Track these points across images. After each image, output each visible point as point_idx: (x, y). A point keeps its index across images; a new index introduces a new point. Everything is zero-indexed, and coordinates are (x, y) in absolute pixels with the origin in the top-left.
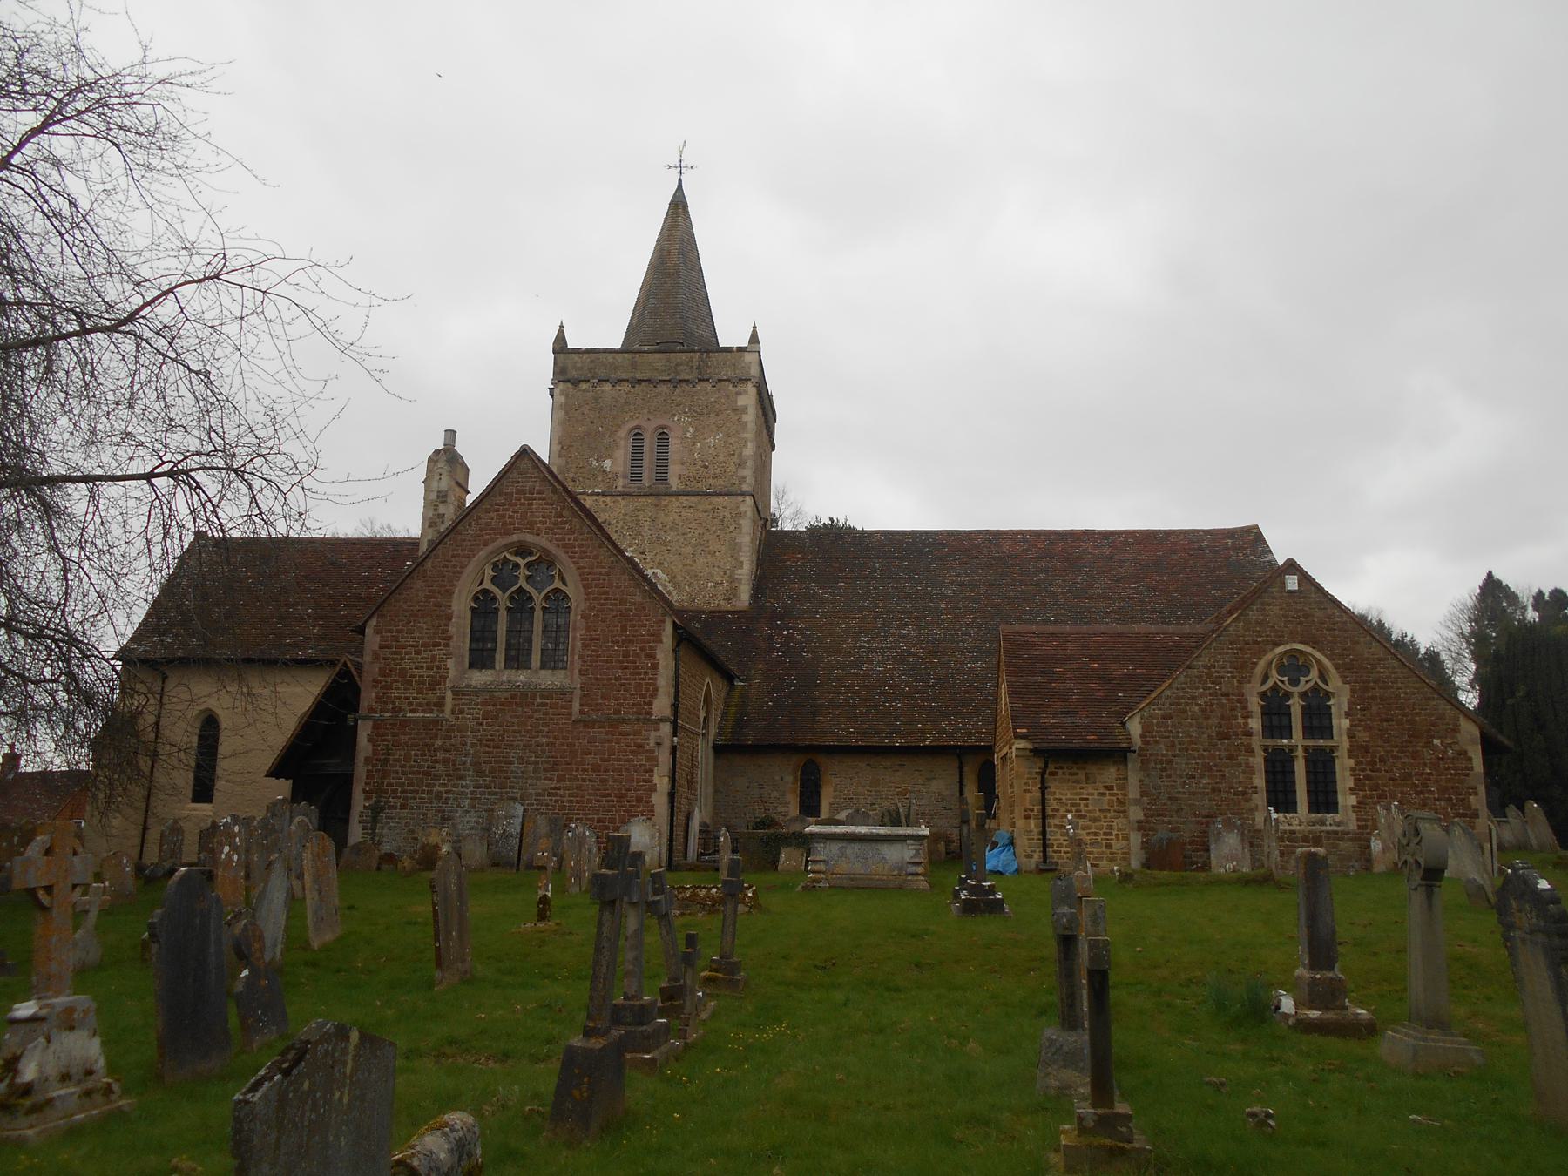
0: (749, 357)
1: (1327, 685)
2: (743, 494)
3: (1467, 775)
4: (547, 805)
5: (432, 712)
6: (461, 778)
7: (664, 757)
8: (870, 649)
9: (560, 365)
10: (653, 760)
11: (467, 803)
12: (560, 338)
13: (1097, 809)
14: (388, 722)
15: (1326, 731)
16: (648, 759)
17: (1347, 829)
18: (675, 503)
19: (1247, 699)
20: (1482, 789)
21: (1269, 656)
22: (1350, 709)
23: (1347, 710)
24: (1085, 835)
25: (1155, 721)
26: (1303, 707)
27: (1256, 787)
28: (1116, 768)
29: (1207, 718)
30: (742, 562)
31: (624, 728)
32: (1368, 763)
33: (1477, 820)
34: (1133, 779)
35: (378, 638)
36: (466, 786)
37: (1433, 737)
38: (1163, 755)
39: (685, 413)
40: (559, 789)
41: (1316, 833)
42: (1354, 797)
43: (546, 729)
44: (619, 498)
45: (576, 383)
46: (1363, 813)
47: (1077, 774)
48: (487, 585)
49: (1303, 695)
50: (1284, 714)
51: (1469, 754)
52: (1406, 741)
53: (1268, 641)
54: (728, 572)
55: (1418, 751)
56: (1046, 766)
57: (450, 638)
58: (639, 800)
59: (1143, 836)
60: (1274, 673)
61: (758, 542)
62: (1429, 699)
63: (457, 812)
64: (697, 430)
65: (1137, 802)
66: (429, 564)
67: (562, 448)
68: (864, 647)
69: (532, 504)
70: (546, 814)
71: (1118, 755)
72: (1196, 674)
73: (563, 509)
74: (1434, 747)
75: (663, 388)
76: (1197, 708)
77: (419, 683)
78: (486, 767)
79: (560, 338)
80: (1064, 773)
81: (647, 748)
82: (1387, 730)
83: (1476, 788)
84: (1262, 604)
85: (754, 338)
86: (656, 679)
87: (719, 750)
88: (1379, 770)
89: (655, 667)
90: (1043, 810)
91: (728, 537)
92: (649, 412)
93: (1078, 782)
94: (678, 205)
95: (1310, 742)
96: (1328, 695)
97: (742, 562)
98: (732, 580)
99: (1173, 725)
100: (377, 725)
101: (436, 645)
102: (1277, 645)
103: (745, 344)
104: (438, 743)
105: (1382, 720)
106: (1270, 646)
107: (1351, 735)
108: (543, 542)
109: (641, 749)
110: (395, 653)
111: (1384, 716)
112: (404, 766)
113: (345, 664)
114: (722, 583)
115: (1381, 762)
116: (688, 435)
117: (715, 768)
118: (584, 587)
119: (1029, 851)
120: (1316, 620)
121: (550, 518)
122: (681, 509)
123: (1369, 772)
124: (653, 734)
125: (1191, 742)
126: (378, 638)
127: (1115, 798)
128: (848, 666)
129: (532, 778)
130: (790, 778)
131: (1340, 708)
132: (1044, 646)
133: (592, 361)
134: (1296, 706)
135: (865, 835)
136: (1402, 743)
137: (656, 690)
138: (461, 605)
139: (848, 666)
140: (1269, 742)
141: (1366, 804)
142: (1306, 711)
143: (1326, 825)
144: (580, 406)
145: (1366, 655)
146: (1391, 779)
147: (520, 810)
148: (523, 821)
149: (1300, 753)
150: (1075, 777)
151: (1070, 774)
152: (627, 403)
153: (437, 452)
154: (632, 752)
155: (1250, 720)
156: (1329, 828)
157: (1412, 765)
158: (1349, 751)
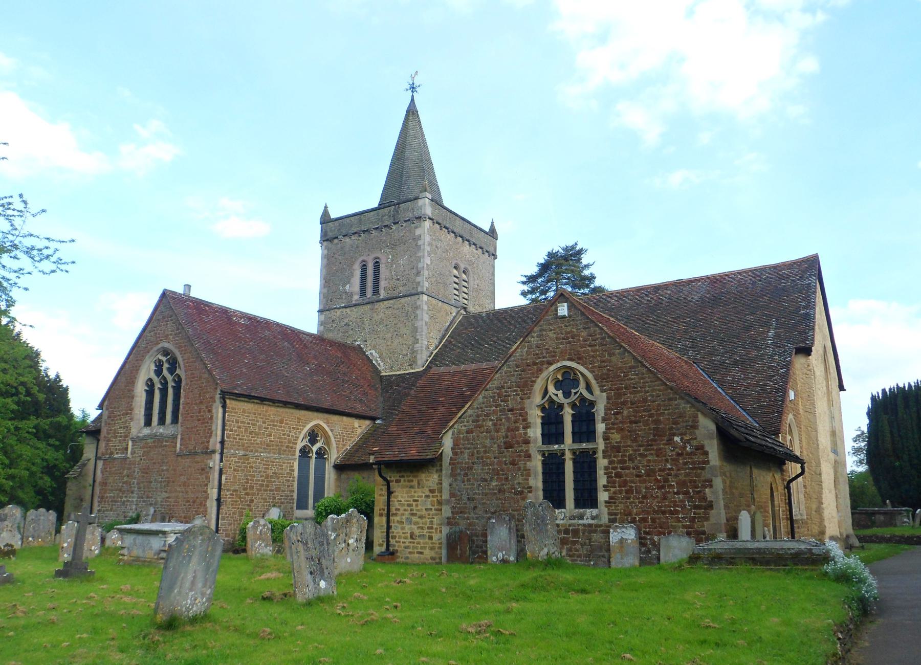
3: (703, 469)
6: (132, 492)
12: (326, 213)
13: (424, 508)
18: (382, 305)
19: (526, 413)
21: (544, 374)
22: (606, 414)
24: (416, 529)
25: (462, 436)
26: (573, 415)
27: (531, 487)
28: (438, 475)
29: (497, 431)
30: (418, 339)
32: (620, 462)
33: (712, 511)
37: (674, 435)
38: (466, 463)
41: (574, 526)
44: (353, 308)
46: (613, 508)
47: (412, 481)
49: (573, 406)
51: (706, 449)
52: (652, 440)
53: (543, 361)
55: (660, 449)
62: (670, 399)
64: (393, 256)
65: (448, 502)
72: (491, 395)
76: (491, 423)
78: (142, 485)
79: (326, 213)
80: (405, 481)
82: (636, 430)
83: (711, 481)
88: (628, 468)
93: (412, 487)
94: (412, 112)
95: (576, 446)
97: (418, 339)
102: (550, 363)
105: (631, 422)
107: (606, 438)
109: (203, 472)
111: (633, 418)
114: (407, 355)
115: (629, 460)
117: (338, 479)
120: (581, 339)
125: (485, 452)
127: (435, 499)
133: (339, 225)
134: (568, 414)
136: (647, 442)
137: (211, 433)
141: (616, 499)
145: (620, 365)
146: (637, 476)
149: (568, 456)
151: (409, 481)
152: (357, 247)
156: (585, 522)
157: (655, 461)
158: (604, 452)
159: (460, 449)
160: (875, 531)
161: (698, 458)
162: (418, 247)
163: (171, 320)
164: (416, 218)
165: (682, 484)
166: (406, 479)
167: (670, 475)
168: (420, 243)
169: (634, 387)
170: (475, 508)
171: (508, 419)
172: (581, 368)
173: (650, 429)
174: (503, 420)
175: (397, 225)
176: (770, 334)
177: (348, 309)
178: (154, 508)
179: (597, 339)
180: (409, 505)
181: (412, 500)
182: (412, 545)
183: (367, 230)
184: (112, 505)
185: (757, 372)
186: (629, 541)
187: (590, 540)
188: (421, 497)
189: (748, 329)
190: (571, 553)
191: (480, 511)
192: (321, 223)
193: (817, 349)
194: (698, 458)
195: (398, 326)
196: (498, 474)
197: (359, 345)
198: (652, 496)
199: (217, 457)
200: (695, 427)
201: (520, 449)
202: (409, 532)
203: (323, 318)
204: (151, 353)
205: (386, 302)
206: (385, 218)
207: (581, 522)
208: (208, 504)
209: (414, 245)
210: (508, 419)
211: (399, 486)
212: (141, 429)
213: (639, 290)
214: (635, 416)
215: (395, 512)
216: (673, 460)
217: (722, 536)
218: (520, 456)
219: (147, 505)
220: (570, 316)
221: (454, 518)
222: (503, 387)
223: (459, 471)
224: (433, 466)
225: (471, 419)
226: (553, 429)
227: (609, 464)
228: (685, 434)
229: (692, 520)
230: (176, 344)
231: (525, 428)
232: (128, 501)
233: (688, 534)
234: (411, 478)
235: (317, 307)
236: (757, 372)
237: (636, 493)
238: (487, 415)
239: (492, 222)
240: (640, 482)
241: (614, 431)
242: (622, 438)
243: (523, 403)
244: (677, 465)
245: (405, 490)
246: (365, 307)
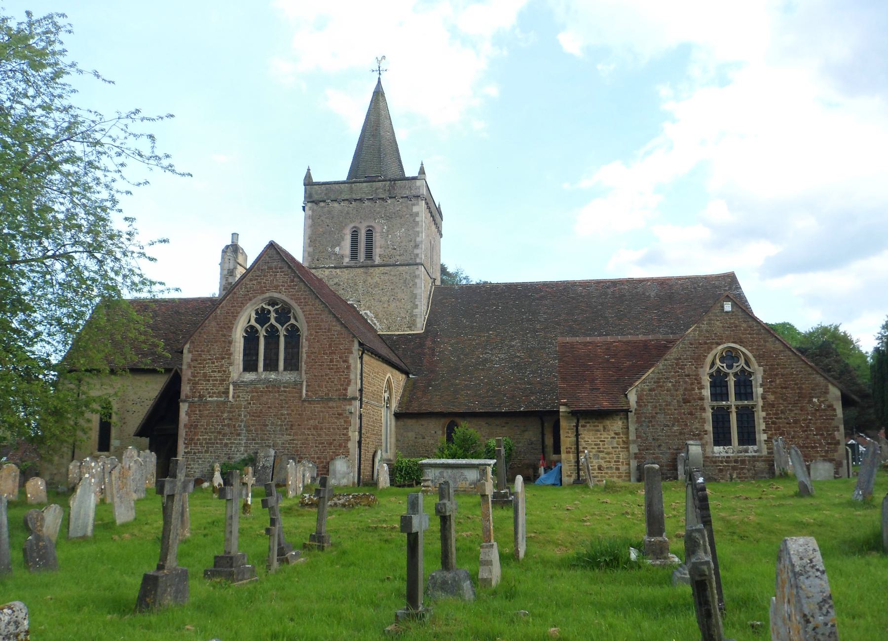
0: (418, 183)
3: (833, 419)
4: (288, 449)
5: (221, 397)
6: (239, 435)
8: (492, 355)
10: (348, 422)
11: (242, 449)
12: (308, 177)
13: (610, 447)
14: (197, 403)
15: (749, 395)
16: (345, 422)
17: (761, 455)
18: (378, 270)
20: (842, 427)
21: (714, 352)
23: (761, 382)
25: (645, 393)
27: (706, 431)
29: (677, 390)
35: (190, 355)
37: (813, 397)
38: (650, 413)
39: (382, 217)
40: (293, 440)
42: (765, 435)
43: (287, 406)
44: (344, 270)
45: (316, 202)
47: (598, 426)
48: (253, 322)
49: (736, 375)
50: (724, 386)
52: (797, 400)
54: (409, 311)
55: (804, 406)
56: (578, 422)
58: (340, 446)
59: (638, 462)
60: (718, 361)
62: (810, 374)
63: (237, 454)
64: (389, 227)
65: (634, 442)
68: (488, 353)
69: (276, 275)
70: (288, 455)
73: (294, 277)
74: (814, 404)
76: (670, 384)
77: (213, 380)
78: (253, 428)
79: (308, 177)
80: (590, 426)
81: (345, 415)
82: (785, 393)
85: (422, 171)
86: (349, 375)
87: (398, 416)
88: (781, 418)
92: (361, 218)
94: (378, 94)
95: (739, 403)
96: (750, 374)
97: (417, 305)
100: (192, 404)
102: (718, 344)
103: (416, 174)
104: (226, 415)
105: (782, 388)
108: (283, 297)
109: (341, 417)
110: (200, 364)
112: (206, 429)
113: (176, 370)
114: (406, 318)
115: (782, 413)
116: (384, 230)
117: (396, 426)
118: (307, 322)
119: (569, 473)
121: (287, 282)
122: (381, 275)
123: (774, 419)
125: (667, 405)
126: (190, 355)
127: (621, 440)
128: (477, 364)
129: (279, 434)
132: (583, 349)
133: (327, 189)
134: (731, 381)
135: (454, 464)
137: (350, 381)
139: (477, 364)
140: (715, 403)
142: (737, 384)
143: (748, 453)
145: (773, 349)
146: (787, 423)
147: (272, 452)
148: (274, 459)
149: (734, 409)
151: (594, 426)
152: (348, 213)
153: (227, 247)
154: (335, 418)
156: (750, 454)
157: (800, 414)
159: (644, 402)
161: (829, 413)
162: (417, 223)
164: (414, 196)
166: (591, 424)
167: (810, 423)
168: (417, 219)
169: (784, 365)
170: (660, 446)
171: (686, 382)
172: (743, 349)
173: (795, 393)
174: (681, 383)
175: (393, 200)
177: (338, 270)
180: (596, 445)
181: (599, 440)
182: (600, 475)
183: (360, 200)
187: (754, 466)
188: (608, 438)
190: (740, 476)
191: (663, 448)
192: (305, 185)
194: (829, 413)
196: (678, 421)
198: (799, 436)
199: (358, 403)
200: (826, 392)
201: (696, 404)
202: (597, 465)
204: (253, 301)
205: (381, 268)
207: (746, 454)
209: (411, 220)
211: (585, 430)
212: (241, 374)
213: (598, 282)
214: (785, 384)
215: (582, 450)
216: (813, 413)
218: (696, 409)
222: (680, 359)
223: (644, 419)
224: (617, 415)
225: (653, 381)
226: (718, 390)
227: (767, 415)
228: (820, 397)
230: (291, 295)
234: (596, 424)
237: (787, 434)
238: (667, 378)
240: (790, 427)
242: (775, 398)
243: (698, 371)
244: (815, 417)
245: (591, 433)
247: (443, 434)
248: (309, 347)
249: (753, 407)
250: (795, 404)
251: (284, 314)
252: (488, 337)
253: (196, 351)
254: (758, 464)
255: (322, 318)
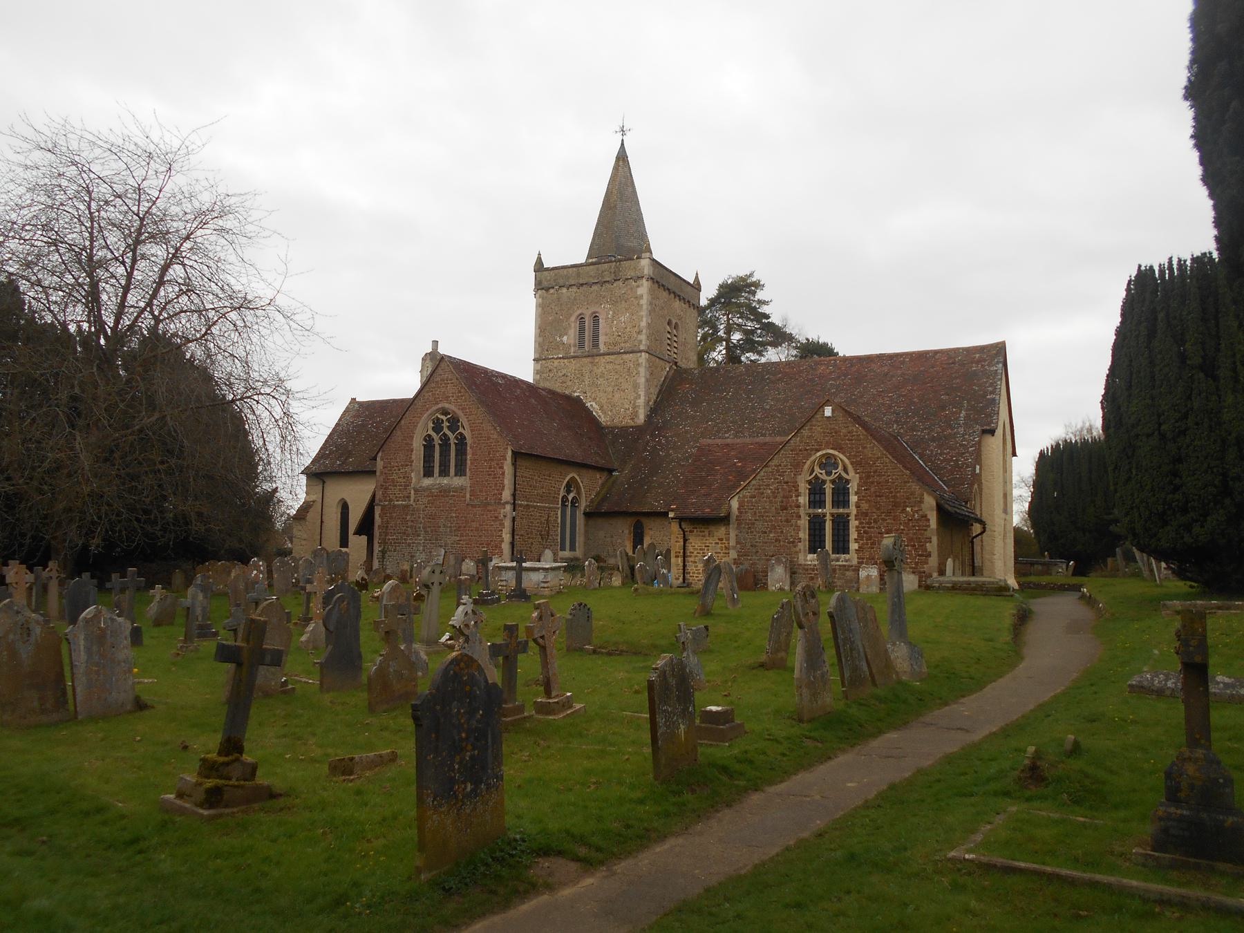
1: (848, 474)
2: (641, 351)
3: (926, 530)
5: (405, 501)
6: (419, 535)
7: (508, 523)
9: (538, 279)
10: (502, 525)
11: (421, 548)
12: (539, 262)
15: (846, 504)
16: (500, 524)
18: (602, 360)
20: (935, 539)
21: (813, 458)
22: (858, 489)
23: (856, 490)
27: (800, 539)
29: (775, 497)
31: (490, 508)
32: (867, 523)
34: (733, 535)
36: (421, 540)
38: (750, 520)
39: (608, 302)
42: (857, 544)
44: (572, 360)
45: (547, 289)
47: (704, 532)
48: (431, 432)
49: (833, 482)
51: (928, 517)
52: (891, 509)
57: (413, 461)
58: (496, 546)
61: (663, 379)
62: (905, 482)
64: (614, 313)
65: (734, 548)
66: (403, 422)
67: (541, 331)
71: (725, 520)
72: (771, 470)
75: (595, 288)
78: (429, 529)
79: (539, 262)
80: (697, 531)
83: (931, 538)
84: (811, 425)
87: (588, 515)
89: (503, 474)
90: (684, 553)
91: (632, 380)
93: (704, 536)
94: (622, 158)
95: (835, 511)
96: (848, 482)
97: (640, 395)
98: (635, 407)
99: (756, 502)
100: (383, 508)
101: (407, 465)
102: (818, 450)
104: (408, 517)
105: (876, 496)
106: (814, 452)
107: (858, 506)
111: (878, 494)
117: (586, 525)
119: (677, 576)
123: (866, 529)
124: (502, 510)
125: (765, 512)
127: (723, 545)
130: (627, 532)
131: (852, 489)
133: (556, 275)
134: (828, 488)
138: (418, 444)
140: (811, 511)
144: (550, 304)
145: (870, 455)
146: (879, 533)
149: (828, 517)
150: (703, 533)
151: (701, 532)
152: (575, 299)
154: (493, 520)
155: (799, 498)
156: (840, 563)
158: (856, 516)
160: (1033, 579)
163: (452, 383)
165: (911, 540)
171: (783, 489)
172: (841, 456)
176: (962, 415)
178: (445, 549)
179: (854, 435)
184: (396, 546)
185: (951, 448)
186: (873, 577)
188: (712, 543)
189: (943, 408)
193: (999, 432)
195: (620, 381)
197: (578, 396)
200: (921, 501)
203: (539, 367)
205: (607, 357)
206: (605, 273)
207: (837, 563)
208: (503, 546)
210: (783, 489)
217: (935, 575)
218: (793, 516)
219: (436, 546)
220: (833, 417)
221: (739, 559)
222: (780, 465)
228: (915, 506)
229: (917, 564)
230: (459, 406)
231: (797, 496)
232: (414, 543)
233: (914, 573)
234: (703, 529)
235: (531, 354)
236: (951, 448)
238: (768, 485)
239: (697, 274)
241: (864, 502)
242: (870, 506)
246: (584, 359)
247: (630, 533)
248: (473, 454)
249: (848, 515)
250: (889, 513)
251: (454, 423)
252: (705, 428)
253: (387, 459)
254: (848, 573)
255: (483, 427)
